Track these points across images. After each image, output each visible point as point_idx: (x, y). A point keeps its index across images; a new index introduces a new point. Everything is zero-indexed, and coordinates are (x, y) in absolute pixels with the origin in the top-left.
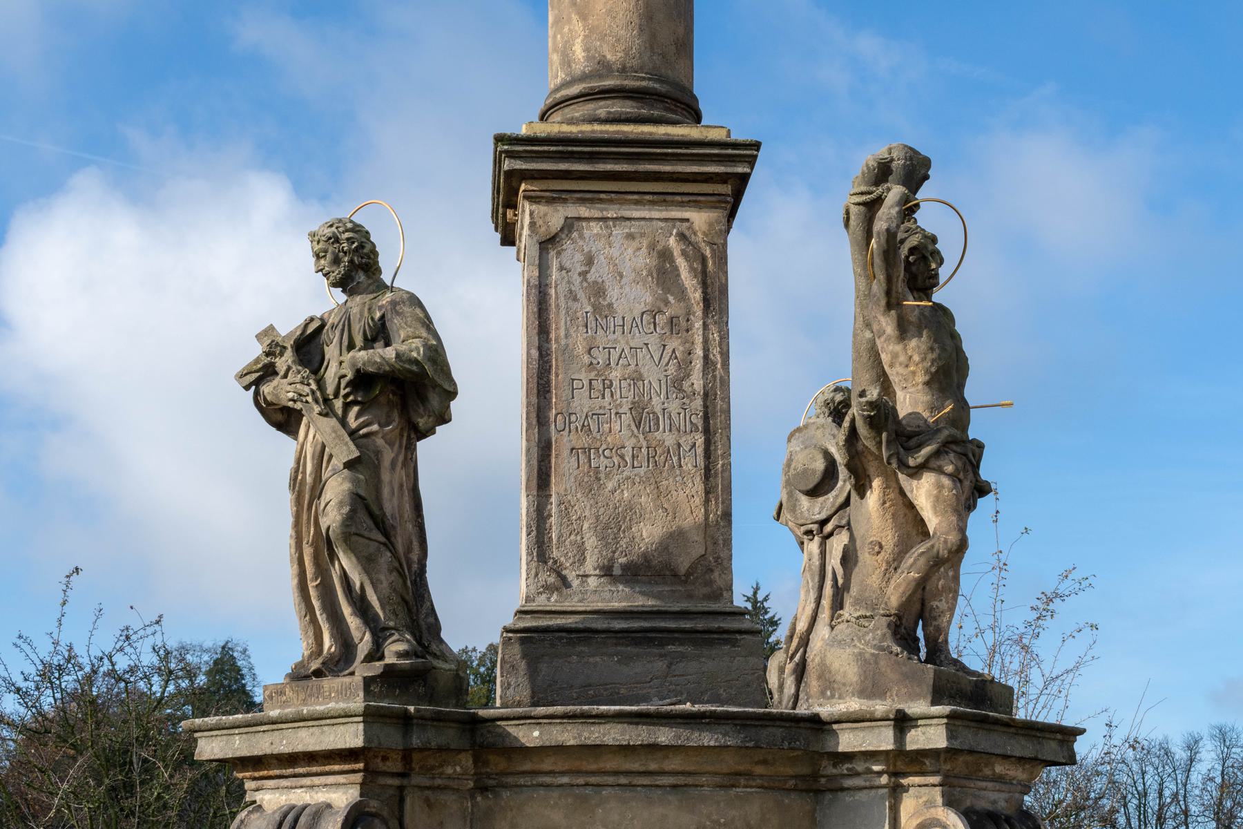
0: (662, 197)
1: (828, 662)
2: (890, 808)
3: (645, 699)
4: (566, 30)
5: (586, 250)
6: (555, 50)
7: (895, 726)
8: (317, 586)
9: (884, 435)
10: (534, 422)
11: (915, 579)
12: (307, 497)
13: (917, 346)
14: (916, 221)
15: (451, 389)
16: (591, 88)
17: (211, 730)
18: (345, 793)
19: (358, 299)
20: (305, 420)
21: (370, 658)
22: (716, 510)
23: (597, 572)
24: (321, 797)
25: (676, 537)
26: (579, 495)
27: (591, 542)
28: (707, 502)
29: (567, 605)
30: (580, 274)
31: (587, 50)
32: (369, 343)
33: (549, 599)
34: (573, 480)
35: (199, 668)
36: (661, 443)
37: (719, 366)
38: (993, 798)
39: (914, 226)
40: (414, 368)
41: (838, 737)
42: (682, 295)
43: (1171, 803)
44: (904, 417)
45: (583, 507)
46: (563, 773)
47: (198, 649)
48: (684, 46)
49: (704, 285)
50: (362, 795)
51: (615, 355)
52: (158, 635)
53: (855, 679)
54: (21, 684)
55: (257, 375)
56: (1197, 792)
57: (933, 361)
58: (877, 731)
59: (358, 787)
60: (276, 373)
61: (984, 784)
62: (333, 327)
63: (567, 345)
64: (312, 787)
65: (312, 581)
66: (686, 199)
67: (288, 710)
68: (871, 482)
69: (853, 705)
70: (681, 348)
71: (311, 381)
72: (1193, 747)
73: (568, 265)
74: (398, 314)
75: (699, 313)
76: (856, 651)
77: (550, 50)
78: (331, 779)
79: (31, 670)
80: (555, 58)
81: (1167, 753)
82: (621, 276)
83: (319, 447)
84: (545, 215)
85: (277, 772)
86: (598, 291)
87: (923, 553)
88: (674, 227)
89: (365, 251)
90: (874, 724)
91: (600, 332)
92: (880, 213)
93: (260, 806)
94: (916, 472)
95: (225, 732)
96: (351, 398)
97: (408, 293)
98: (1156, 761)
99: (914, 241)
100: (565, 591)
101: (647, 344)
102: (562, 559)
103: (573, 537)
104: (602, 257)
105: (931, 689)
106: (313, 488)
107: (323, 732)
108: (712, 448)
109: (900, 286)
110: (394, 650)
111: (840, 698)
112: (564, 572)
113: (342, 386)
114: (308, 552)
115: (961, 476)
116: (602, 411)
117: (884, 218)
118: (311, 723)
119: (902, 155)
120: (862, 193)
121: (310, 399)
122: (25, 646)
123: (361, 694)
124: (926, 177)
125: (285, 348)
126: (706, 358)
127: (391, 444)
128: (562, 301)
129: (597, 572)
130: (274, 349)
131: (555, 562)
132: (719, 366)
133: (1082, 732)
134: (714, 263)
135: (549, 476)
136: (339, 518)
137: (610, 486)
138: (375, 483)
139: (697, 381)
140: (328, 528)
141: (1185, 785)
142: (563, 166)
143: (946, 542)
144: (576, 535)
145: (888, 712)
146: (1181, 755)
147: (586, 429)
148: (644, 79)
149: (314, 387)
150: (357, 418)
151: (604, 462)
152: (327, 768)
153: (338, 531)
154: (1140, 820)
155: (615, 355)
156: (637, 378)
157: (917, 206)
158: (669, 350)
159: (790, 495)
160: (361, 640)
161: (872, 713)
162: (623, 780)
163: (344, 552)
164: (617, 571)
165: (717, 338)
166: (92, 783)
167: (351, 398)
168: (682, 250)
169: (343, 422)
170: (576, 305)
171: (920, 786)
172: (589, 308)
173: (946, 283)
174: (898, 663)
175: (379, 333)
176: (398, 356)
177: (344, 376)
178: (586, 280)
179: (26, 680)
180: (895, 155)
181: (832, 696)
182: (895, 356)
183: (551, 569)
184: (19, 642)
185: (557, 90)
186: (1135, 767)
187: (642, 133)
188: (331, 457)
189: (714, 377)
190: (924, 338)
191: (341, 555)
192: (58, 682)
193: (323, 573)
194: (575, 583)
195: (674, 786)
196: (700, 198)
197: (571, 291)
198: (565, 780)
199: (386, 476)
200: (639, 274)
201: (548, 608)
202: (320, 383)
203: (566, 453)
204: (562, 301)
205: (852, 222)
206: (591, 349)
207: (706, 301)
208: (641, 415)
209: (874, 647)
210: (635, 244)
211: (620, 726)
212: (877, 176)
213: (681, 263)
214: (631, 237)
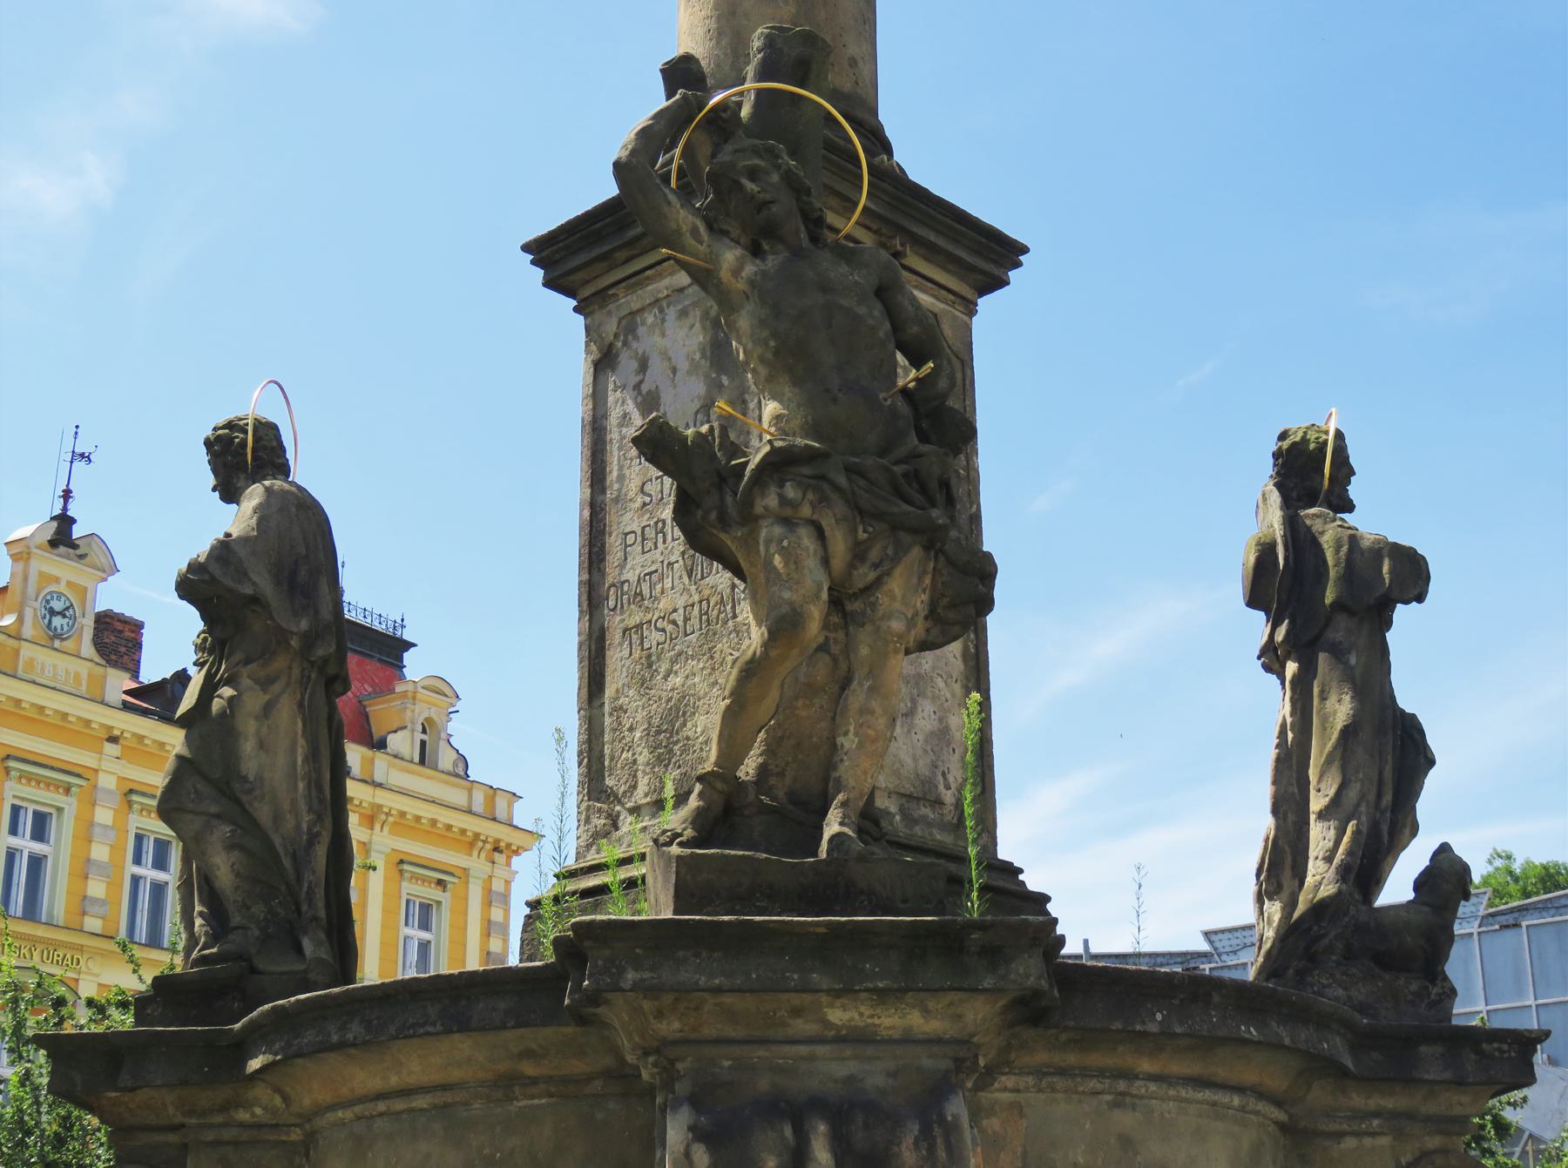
103: (624, 756)
133: (414, 645)
144: (628, 751)
178: (640, 393)
206: (644, 484)
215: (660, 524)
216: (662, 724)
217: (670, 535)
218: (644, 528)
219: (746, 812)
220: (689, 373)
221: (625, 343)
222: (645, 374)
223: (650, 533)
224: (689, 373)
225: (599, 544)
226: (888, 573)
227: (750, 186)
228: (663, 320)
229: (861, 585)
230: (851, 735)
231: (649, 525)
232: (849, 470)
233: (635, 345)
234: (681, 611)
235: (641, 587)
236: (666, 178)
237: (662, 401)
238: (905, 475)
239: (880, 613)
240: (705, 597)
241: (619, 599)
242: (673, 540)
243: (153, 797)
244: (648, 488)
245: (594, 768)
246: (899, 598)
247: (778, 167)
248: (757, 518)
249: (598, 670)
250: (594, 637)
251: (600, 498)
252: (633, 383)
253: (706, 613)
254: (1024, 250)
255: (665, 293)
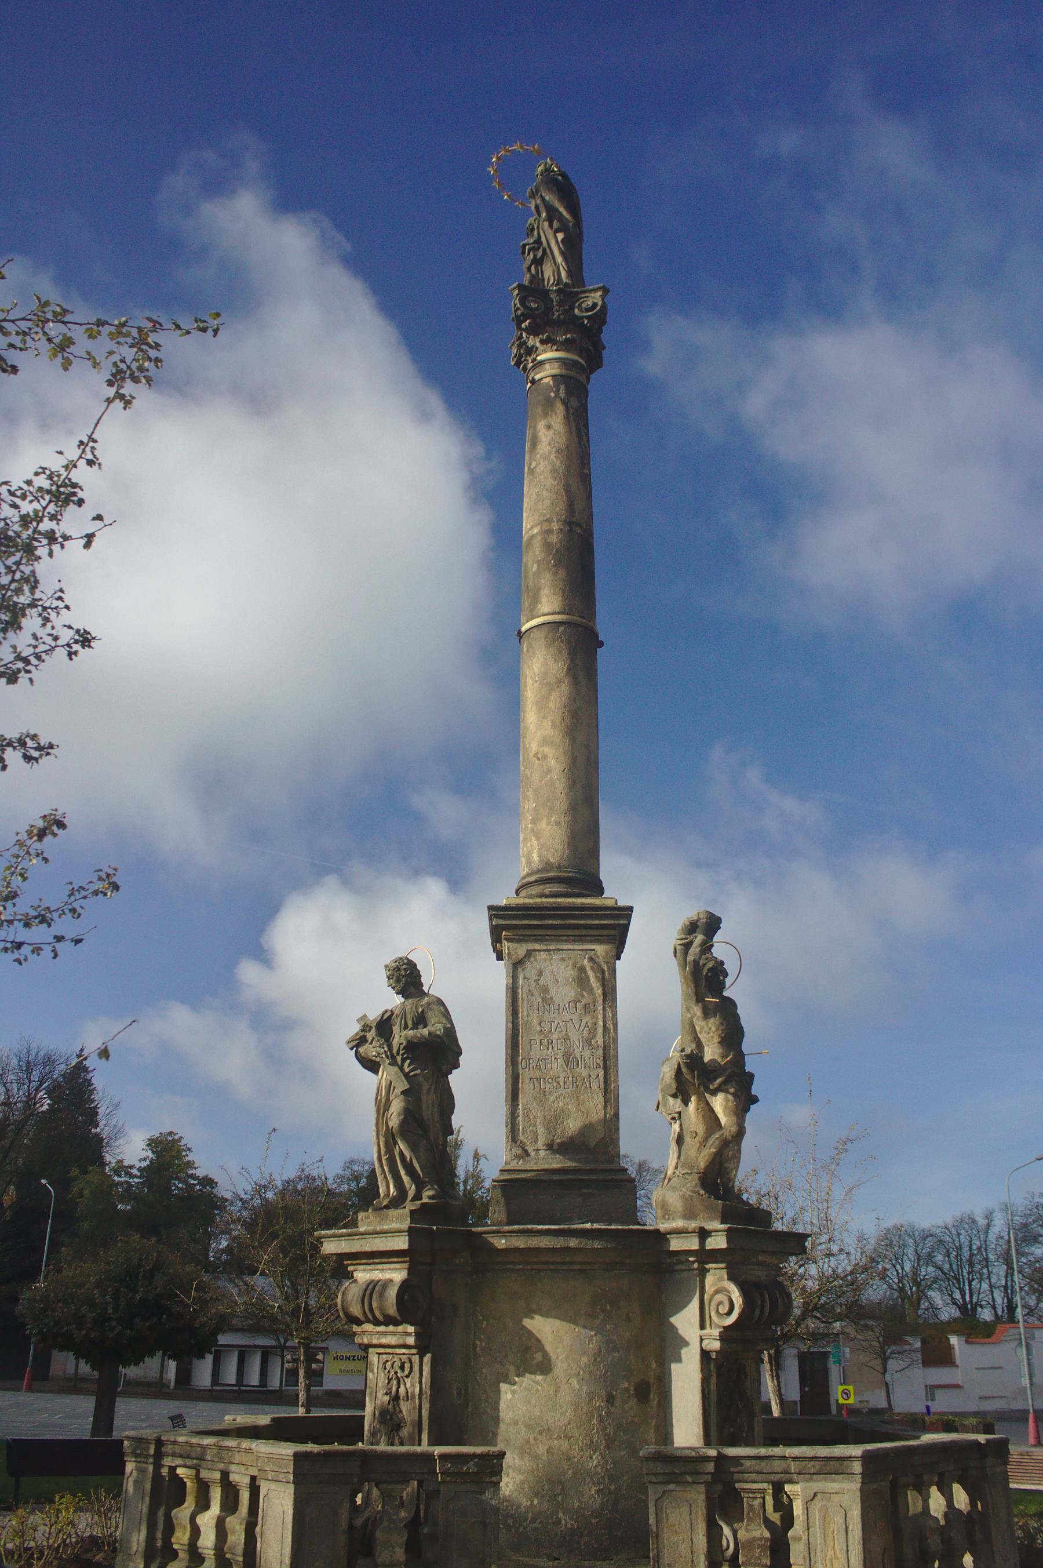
0: (579, 938)
1: (666, 1200)
2: (700, 1281)
3: (570, 1220)
4: (529, 845)
5: (538, 967)
6: (523, 856)
7: (699, 1237)
8: (387, 1159)
9: (696, 1072)
10: (510, 1064)
11: (713, 1153)
12: (382, 1110)
13: (713, 1022)
14: (712, 953)
15: (459, 1051)
16: (543, 877)
17: (330, 1237)
18: (400, 1274)
19: (410, 1001)
20: (382, 1067)
21: (414, 1199)
22: (610, 1112)
23: (545, 1147)
24: (387, 1275)
25: (587, 1129)
26: (534, 1104)
27: (541, 1131)
28: (605, 1107)
29: (528, 1167)
30: (535, 981)
31: (539, 856)
32: (415, 1026)
33: (518, 1163)
34: (531, 1096)
35: (363, 1174)
36: (580, 1075)
37: (612, 1031)
38: (759, 1274)
39: (711, 956)
40: (438, 1040)
41: (670, 1243)
42: (591, 991)
43: (977, 1254)
44: (708, 1062)
45: (536, 1111)
46: (519, 1263)
47: (362, 1162)
48: (594, 853)
49: (603, 986)
50: (408, 1275)
51: (554, 1026)
52: (321, 1169)
53: (680, 1209)
54: (243, 1196)
55: (357, 1042)
56: (993, 1246)
57: (722, 1030)
58: (690, 1238)
59: (407, 1271)
60: (367, 1041)
61: (751, 1267)
62: (397, 1016)
63: (528, 1021)
64: (383, 1270)
65: (384, 1156)
66: (593, 938)
67: (369, 1228)
68: (691, 1097)
69: (679, 1223)
70: (591, 1022)
71: (385, 1046)
72: (989, 1216)
73: (528, 976)
74: (431, 1009)
75: (601, 1001)
76: (681, 1193)
77: (521, 855)
78: (393, 1266)
79: (249, 1188)
80: (523, 860)
81: (974, 1221)
82: (558, 982)
83: (389, 1082)
84: (516, 948)
85: (364, 1261)
86: (545, 990)
87: (717, 1138)
88: (586, 954)
89: (414, 975)
90: (688, 1235)
91: (546, 1012)
92: (690, 951)
93: (356, 1280)
94: (714, 1093)
95: (337, 1239)
96: (405, 1056)
97: (436, 997)
98: (966, 1226)
99: (710, 965)
100: (527, 1159)
101: (572, 1020)
102: (525, 1140)
104: (547, 972)
105: (720, 1215)
106: (385, 1104)
107: (387, 1241)
108: (608, 1077)
109: (703, 989)
110: (427, 1193)
111: (673, 1219)
112: (526, 1148)
113: (401, 1049)
114: (382, 1140)
115: (739, 1094)
116: (547, 1057)
117: (693, 953)
118: (381, 1235)
119: (705, 917)
120: (682, 939)
121: (384, 1056)
122: (246, 1174)
123: (409, 1219)
124: (720, 928)
125: (371, 1027)
126: (604, 1026)
127: (427, 1080)
128: (525, 995)
129: (545, 1147)
130: (366, 1028)
131: (521, 1142)
132: (612, 1031)
134: (609, 973)
135: (518, 1094)
136: (398, 1122)
137: (552, 1099)
138: (418, 1100)
139: (599, 1039)
140: (392, 1128)
141: (985, 1241)
142: (525, 922)
143: (730, 1132)
145: (695, 1228)
146: (982, 1222)
147: (538, 1067)
148: (570, 872)
149: (386, 1049)
150: (409, 1066)
151: (548, 1086)
152: (391, 1260)
153: (397, 1130)
154: (958, 1265)
155: (554, 1026)
156: (566, 1038)
157: (712, 946)
158: (584, 1022)
159: (664, 1097)
160: (410, 1188)
161: (687, 1229)
162: (552, 1267)
163: (401, 1140)
164: (555, 1147)
165: (611, 1016)
166: (281, 1256)
167: (405, 1056)
168: (591, 967)
169: (401, 1068)
170: (532, 999)
171: (715, 1269)
172: (540, 1000)
173: (730, 987)
174: (703, 1200)
175: (421, 1020)
176: (430, 1033)
177: (401, 1044)
178: (538, 984)
179: (246, 1194)
180: (701, 916)
181: (669, 1219)
182: (702, 1028)
183: (519, 1146)
184: (242, 1171)
185: (524, 878)
186: (954, 1231)
187: (569, 903)
188: (394, 1088)
189: (609, 1037)
190: (718, 1018)
191: (399, 1142)
192: (264, 1195)
193: (390, 1150)
194: (533, 1154)
195: (580, 1270)
196: (600, 938)
197: (530, 990)
198: (520, 1267)
199: (424, 1098)
200: (568, 980)
201: (517, 1168)
202: (390, 1047)
203: (527, 1081)
204: (525, 995)
205: (678, 954)
207: (605, 995)
208: (568, 1058)
209: (691, 1191)
210: (566, 963)
211: (548, 1237)
212: (689, 929)
213: (590, 973)
214: (563, 959)
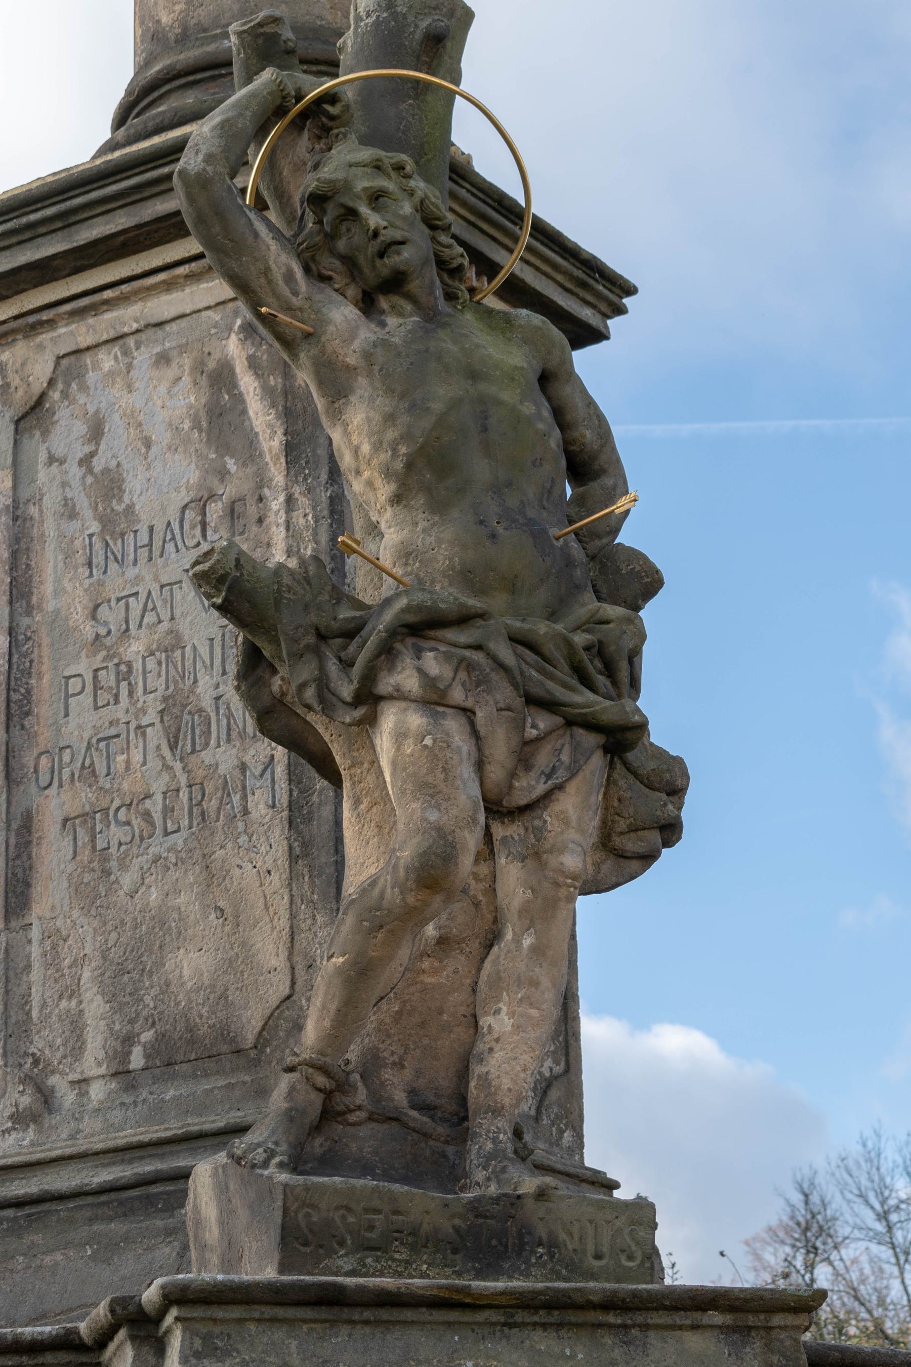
144: (70, 998)
178: (90, 471)
206: (97, 607)
215: (123, 668)
216: (126, 960)
217: (140, 684)
218: (96, 671)
219: (352, 1118)
220: (172, 449)
221: (65, 395)
222: (98, 444)
223: (108, 678)
224: (172, 449)
225: (23, 691)
226: (560, 787)
227: (374, 220)
228: (129, 367)
229: (523, 801)
230: (503, 1015)
231: (106, 667)
232: (517, 640)
233: (82, 399)
234: (159, 797)
235: (92, 757)
236: (243, 191)
237: (127, 486)
238: (587, 648)
239: (547, 846)
240: (198, 781)
241: (56, 773)
242: (145, 692)
243: (228, 1264)
244: (103, 612)
245: (13, 1020)
246: (574, 824)
247: (411, 193)
248: (380, 698)
249: (20, 875)
250: (14, 826)
251: (25, 621)
252: (80, 455)
253: (199, 804)
254: (630, 290)
255: (135, 326)
